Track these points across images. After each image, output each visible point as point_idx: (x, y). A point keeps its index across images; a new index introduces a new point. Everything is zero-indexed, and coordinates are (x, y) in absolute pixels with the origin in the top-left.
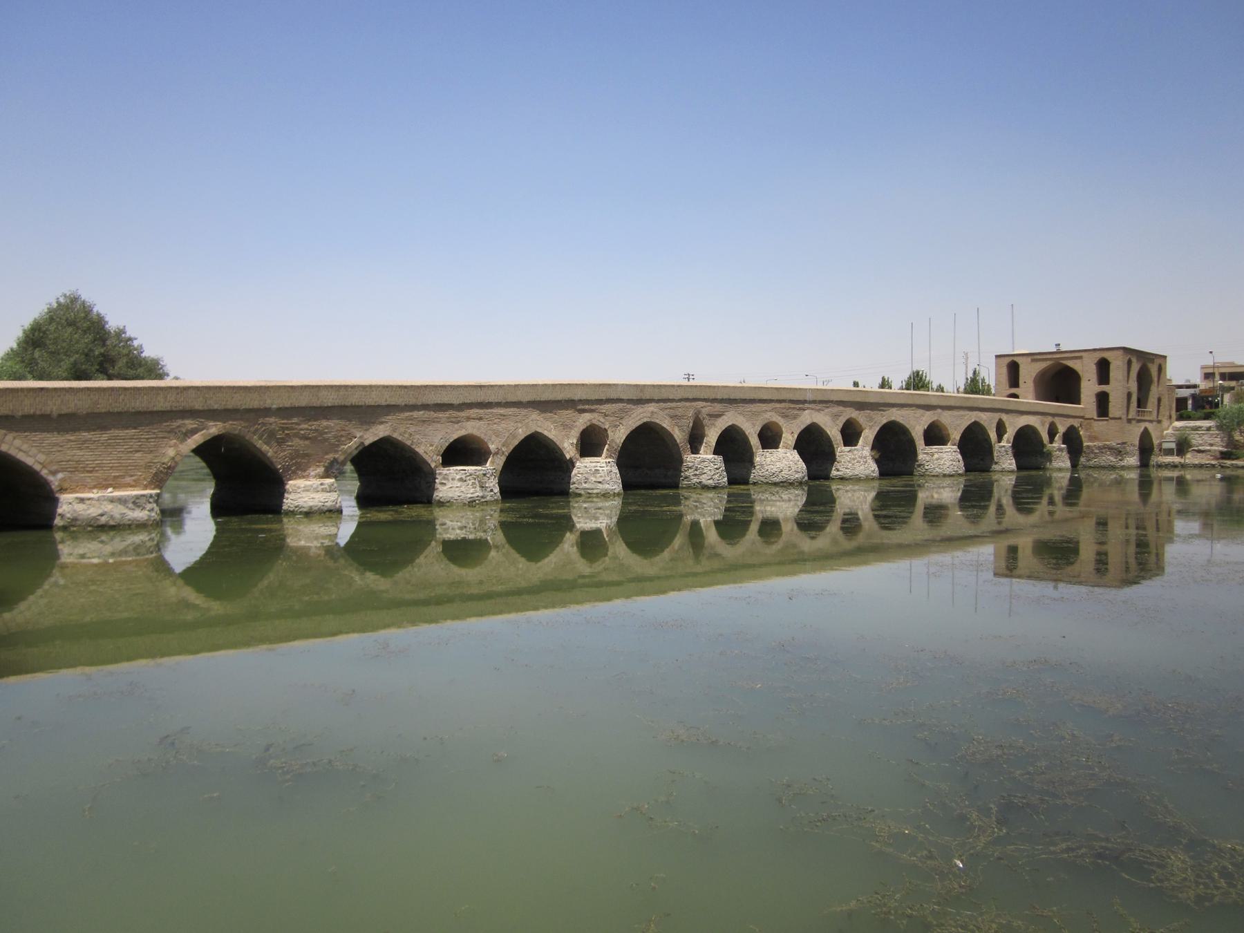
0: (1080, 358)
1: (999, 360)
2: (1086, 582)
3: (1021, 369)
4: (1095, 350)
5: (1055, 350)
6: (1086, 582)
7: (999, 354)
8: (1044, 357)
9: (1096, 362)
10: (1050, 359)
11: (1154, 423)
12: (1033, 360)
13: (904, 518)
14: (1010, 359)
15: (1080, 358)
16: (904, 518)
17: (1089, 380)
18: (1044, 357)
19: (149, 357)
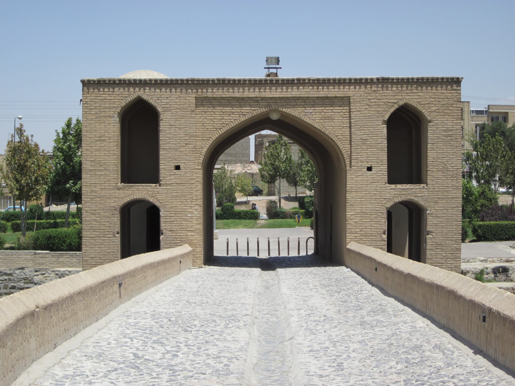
0: (345, 101)
1: (94, 93)
2: (101, 284)
3: (163, 126)
4: (384, 82)
5: (261, 75)
6: (101, 284)
7: (95, 77)
8: (238, 93)
9: (386, 117)
10: (256, 101)
11: (467, 278)
12: (201, 102)
13: (65, 382)
14: (133, 94)
15: (345, 101)
16: (65, 382)
17: (369, 169)
18: (238, 93)
19: (292, 186)
